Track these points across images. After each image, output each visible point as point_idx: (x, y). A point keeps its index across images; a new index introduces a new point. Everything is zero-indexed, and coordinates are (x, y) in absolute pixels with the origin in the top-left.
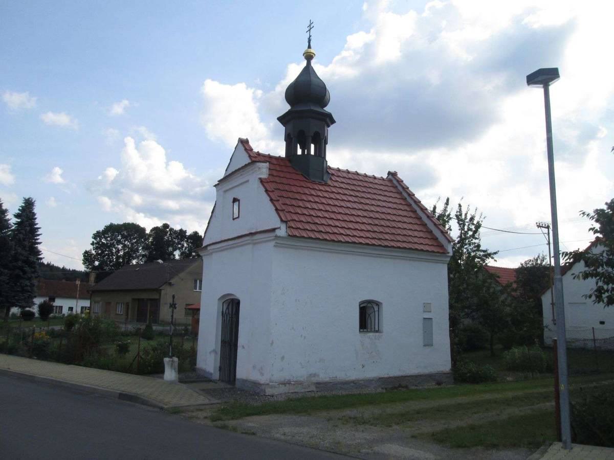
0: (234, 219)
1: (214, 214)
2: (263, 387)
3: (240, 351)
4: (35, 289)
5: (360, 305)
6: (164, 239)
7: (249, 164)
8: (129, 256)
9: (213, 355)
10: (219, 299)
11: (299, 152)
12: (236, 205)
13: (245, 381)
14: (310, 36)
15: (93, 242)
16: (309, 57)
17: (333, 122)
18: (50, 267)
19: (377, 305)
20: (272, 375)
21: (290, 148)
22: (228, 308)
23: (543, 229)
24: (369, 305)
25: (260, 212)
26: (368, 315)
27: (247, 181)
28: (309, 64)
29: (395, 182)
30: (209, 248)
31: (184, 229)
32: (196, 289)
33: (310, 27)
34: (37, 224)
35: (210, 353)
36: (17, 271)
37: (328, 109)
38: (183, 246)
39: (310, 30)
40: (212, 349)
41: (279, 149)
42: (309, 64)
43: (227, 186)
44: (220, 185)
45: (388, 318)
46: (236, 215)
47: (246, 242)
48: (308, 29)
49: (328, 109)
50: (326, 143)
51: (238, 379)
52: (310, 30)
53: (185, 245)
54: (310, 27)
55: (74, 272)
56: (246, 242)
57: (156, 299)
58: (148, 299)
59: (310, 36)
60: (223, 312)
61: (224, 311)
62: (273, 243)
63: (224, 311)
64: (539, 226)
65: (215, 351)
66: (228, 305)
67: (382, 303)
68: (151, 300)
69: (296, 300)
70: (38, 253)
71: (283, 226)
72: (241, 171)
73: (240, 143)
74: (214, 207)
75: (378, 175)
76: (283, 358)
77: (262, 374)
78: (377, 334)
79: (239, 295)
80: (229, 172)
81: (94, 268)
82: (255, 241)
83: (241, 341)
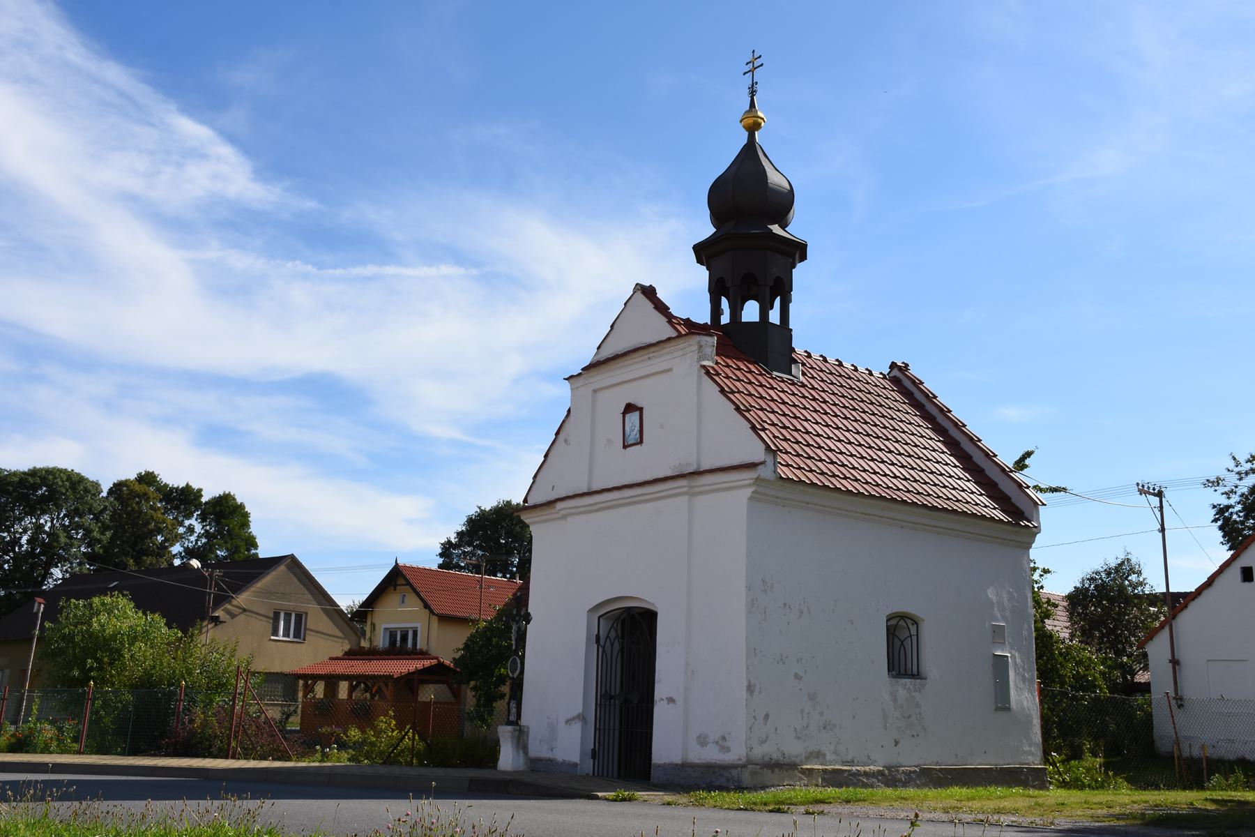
0: (625, 447)
2: (735, 773)
7: (669, 339)
9: (577, 726)
10: (591, 611)
12: (633, 418)
16: (753, 128)
20: (751, 749)
21: (716, 312)
23: (1151, 498)
24: (902, 623)
26: (902, 647)
27: (671, 370)
31: (195, 486)
32: (275, 633)
33: (753, 66)
35: (568, 722)
38: (191, 530)
39: (752, 71)
44: (581, 378)
45: (933, 650)
46: (633, 436)
52: (752, 71)
54: (753, 66)
60: (598, 637)
62: (748, 492)
64: (1141, 492)
65: (582, 718)
76: (767, 717)
80: (607, 352)
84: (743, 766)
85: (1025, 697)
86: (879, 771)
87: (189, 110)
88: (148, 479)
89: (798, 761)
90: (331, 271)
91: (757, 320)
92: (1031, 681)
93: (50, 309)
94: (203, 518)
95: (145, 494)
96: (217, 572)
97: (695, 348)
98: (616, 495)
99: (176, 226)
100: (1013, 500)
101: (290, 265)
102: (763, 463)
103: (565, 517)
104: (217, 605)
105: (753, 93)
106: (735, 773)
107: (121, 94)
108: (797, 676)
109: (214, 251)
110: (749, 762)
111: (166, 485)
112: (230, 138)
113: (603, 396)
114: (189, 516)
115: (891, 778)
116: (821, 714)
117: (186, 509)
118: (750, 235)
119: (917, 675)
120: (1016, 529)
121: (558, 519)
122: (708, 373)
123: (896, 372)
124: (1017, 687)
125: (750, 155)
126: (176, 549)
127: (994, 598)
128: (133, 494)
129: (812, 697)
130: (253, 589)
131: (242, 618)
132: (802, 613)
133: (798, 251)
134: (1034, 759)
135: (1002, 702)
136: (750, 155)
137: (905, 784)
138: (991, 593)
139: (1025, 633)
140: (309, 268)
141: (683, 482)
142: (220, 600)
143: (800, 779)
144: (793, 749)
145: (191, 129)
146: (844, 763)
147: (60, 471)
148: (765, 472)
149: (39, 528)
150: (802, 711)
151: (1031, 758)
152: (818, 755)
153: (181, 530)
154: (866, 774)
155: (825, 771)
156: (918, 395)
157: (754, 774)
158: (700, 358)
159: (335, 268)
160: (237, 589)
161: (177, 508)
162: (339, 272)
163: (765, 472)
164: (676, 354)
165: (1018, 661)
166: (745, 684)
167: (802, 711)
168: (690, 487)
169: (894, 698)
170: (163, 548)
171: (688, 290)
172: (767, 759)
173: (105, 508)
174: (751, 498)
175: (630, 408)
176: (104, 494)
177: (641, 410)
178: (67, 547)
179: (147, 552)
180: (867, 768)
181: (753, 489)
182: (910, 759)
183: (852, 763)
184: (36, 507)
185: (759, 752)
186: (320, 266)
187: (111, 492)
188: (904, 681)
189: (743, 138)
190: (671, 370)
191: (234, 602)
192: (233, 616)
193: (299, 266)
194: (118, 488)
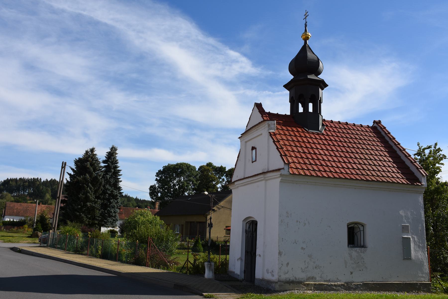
0: (252, 162)
1: (239, 158)
3: (258, 258)
4: (117, 215)
5: (348, 226)
6: (209, 173)
7: (262, 122)
8: (183, 188)
9: (239, 261)
11: (301, 110)
12: (254, 151)
13: (263, 280)
14: (306, 22)
15: (157, 179)
16: (306, 39)
17: (326, 85)
18: (128, 198)
19: (362, 226)
20: (280, 276)
21: (294, 108)
22: (249, 227)
24: (356, 226)
25: (271, 157)
26: (354, 235)
27: (262, 134)
28: (306, 43)
29: (379, 128)
30: (236, 183)
31: (224, 166)
34: (118, 167)
35: (238, 260)
36: (106, 202)
37: (321, 77)
38: (223, 180)
40: (239, 257)
41: (284, 109)
42: (306, 43)
43: (247, 138)
45: (370, 236)
46: (254, 160)
47: (260, 179)
48: (304, 17)
49: (321, 77)
50: (320, 102)
51: (257, 279)
53: (225, 180)
55: (144, 201)
56: (260, 179)
57: (203, 222)
58: (197, 222)
59: (306, 22)
60: (246, 230)
61: (247, 229)
62: (279, 179)
63: (247, 229)
65: (241, 259)
66: (250, 225)
67: (365, 225)
68: (200, 222)
69: (297, 221)
70: (119, 189)
71: (286, 167)
72: (257, 127)
73: (256, 107)
74: (239, 153)
75: (365, 124)
76: (288, 264)
77: (273, 275)
78: (363, 249)
79: (256, 218)
80: (249, 128)
81: (158, 199)
82: (267, 178)
83: (258, 252)
84: (276, 283)
85: (419, 254)
86: (342, 285)
87: (232, 48)
88: (209, 165)
89: (302, 280)
90: (277, 93)
91: (288, 113)
92: (423, 248)
93: (196, 113)
94: (226, 176)
95: (208, 169)
96: (213, 195)
97: (267, 126)
98: (250, 179)
99: (230, 84)
100: (415, 174)
101: (264, 92)
102: (283, 169)
103: (238, 187)
104: (214, 207)
105: (306, 26)
106: (273, 285)
107: (213, 46)
108: (302, 248)
109: (242, 91)
110: (279, 281)
111: (215, 166)
112: (245, 55)
113: (248, 143)
114: (223, 176)
115: (348, 287)
116: (314, 262)
117: (221, 174)
118: (305, 80)
119: (364, 246)
120: (413, 186)
121: (236, 188)
122: (271, 135)
123: (375, 125)
124: (415, 250)
125: (305, 49)
126: (219, 185)
127: (403, 214)
128: (205, 170)
129: (310, 256)
130: (225, 200)
131: (222, 210)
132: (305, 224)
133: (323, 85)
134: (425, 280)
135: (407, 255)
136: (305, 49)
137: (355, 289)
138: (402, 213)
139: (420, 228)
140: (270, 93)
141: (262, 176)
142: (216, 203)
143: (303, 287)
144: (300, 276)
145: (233, 54)
146: (325, 281)
147: (184, 163)
148: (285, 172)
149: (180, 180)
150: (305, 262)
151: (423, 279)
152: (313, 278)
153: (221, 180)
154: (335, 285)
155: (315, 284)
156: (383, 133)
157: (280, 286)
158: (269, 129)
159: (278, 92)
160: (220, 200)
161: (219, 173)
162: (279, 93)
163: (285, 172)
164: (263, 128)
165: (416, 239)
166: (278, 252)
167: (305, 262)
168: (265, 178)
169: (351, 256)
170: (215, 186)
171: (279, 103)
172: (288, 280)
173: (197, 174)
174: (280, 182)
175: (253, 148)
176: (197, 170)
177: (256, 148)
178: (187, 186)
179: (209, 187)
180: (336, 283)
181: (281, 178)
182: (358, 279)
183: (329, 281)
184: (178, 175)
185: (284, 277)
186: (274, 92)
187: (199, 169)
188: (355, 249)
189: (303, 43)
190: (262, 134)
191: (219, 205)
192: (219, 209)
193: (267, 92)
194: (201, 167)
